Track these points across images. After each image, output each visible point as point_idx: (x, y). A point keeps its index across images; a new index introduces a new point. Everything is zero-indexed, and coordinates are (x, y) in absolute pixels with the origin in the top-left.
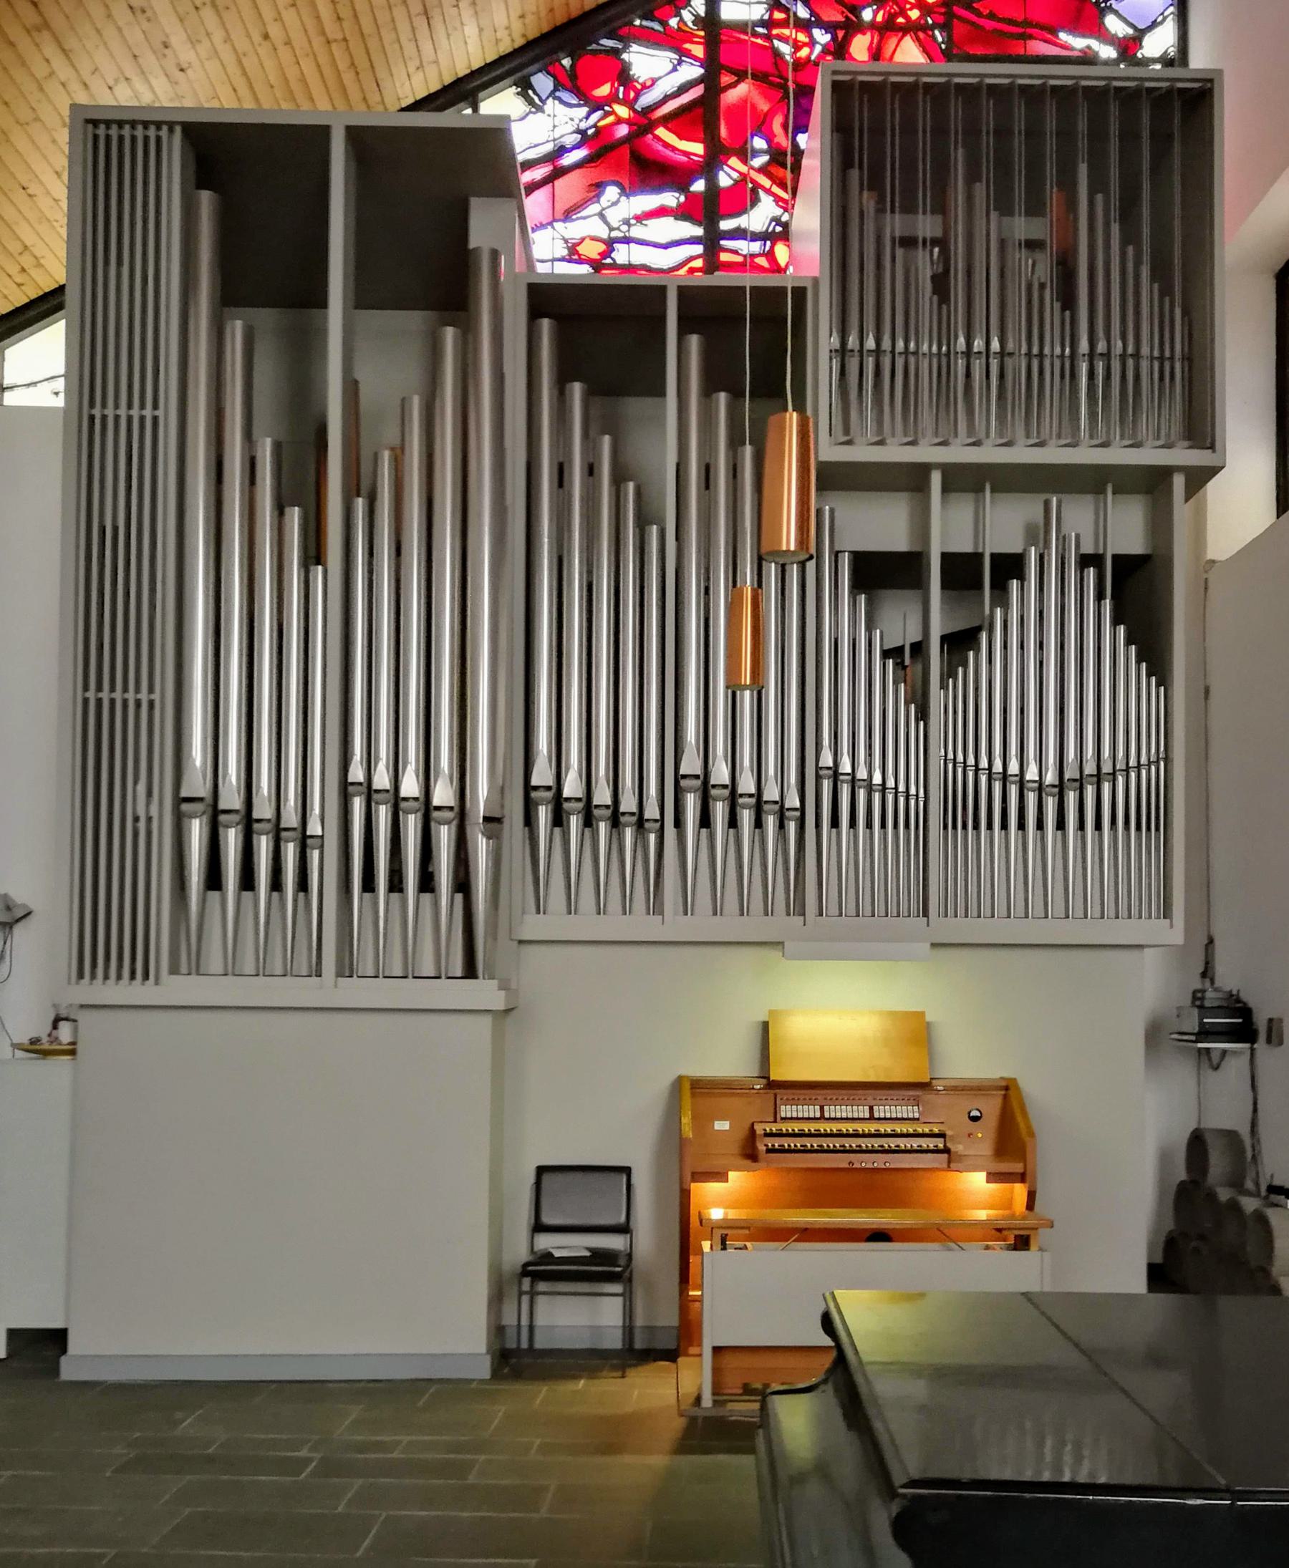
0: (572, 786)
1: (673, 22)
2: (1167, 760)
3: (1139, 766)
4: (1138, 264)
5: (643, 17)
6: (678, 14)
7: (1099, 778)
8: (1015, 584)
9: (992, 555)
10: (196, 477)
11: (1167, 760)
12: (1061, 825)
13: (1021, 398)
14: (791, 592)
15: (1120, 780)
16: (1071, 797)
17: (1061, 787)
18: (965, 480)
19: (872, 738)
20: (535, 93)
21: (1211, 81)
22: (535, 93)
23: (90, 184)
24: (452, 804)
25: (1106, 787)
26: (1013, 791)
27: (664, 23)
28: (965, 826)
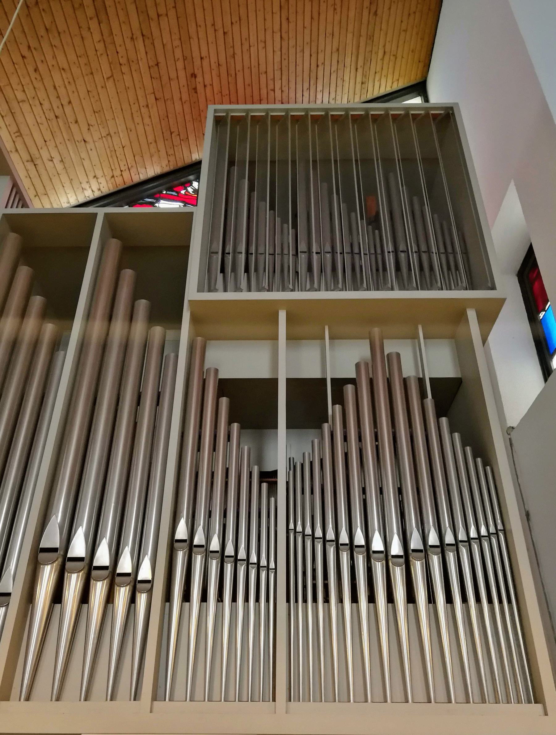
1: (183, 192)
2: (504, 531)
4: (422, 204)
5: (167, 190)
6: (185, 188)
9: (333, 380)
11: (504, 531)
16: (418, 567)
17: (406, 557)
21: (452, 108)
23: (211, 459)
26: (360, 561)
27: (178, 193)
28: (315, 600)
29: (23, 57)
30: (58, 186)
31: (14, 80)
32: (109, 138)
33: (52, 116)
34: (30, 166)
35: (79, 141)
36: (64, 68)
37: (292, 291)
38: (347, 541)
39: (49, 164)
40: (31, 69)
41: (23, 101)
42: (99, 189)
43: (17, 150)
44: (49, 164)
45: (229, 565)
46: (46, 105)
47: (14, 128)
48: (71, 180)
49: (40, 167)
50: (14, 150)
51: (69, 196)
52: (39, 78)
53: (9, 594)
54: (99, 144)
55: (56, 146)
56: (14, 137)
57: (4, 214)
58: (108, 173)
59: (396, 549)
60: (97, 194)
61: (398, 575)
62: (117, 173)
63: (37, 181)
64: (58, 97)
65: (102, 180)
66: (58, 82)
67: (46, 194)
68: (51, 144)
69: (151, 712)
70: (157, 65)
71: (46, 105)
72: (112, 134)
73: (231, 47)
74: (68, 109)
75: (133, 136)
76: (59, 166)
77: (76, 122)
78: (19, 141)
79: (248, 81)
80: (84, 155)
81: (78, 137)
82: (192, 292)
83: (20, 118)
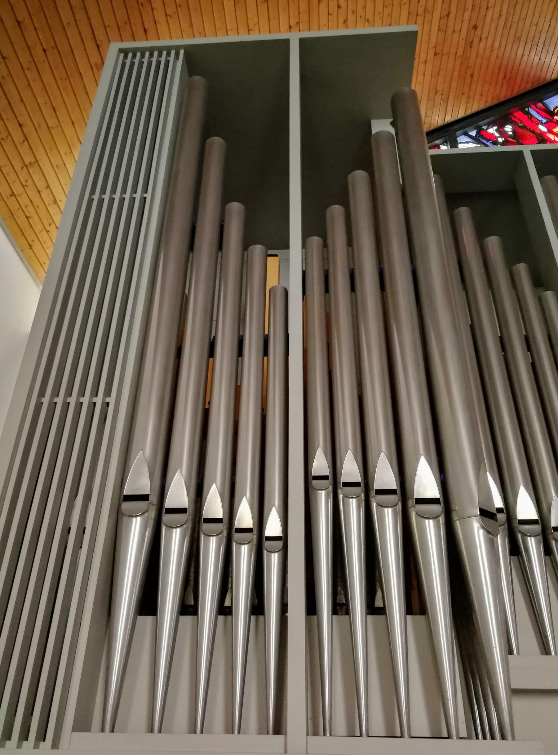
35: (5, 137)
36: (369, 19)
38: (357, 477)
45: (213, 541)
69: (546, 651)
70: (448, 15)
73: (386, 7)
79: (519, 34)
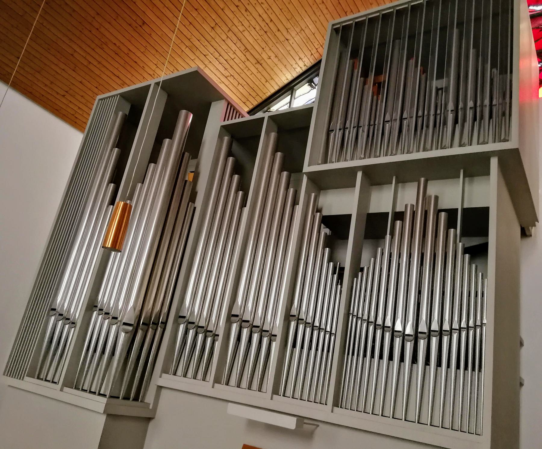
0: (328, 329)
3: (468, 328)
7: (441, 333)
8: (167, 141)
10: (92, 196)
12: (414, 360)
13: (429, 124)
14: (448, 266)
15: (455, 336)
16: (422, 344)
18: (402, 173)
19: (322, 301)
20: (314, 83)
22: (314, 83)
24: (133, 323)
25: (445, 339)
26: (388, 336)
29: (237, 6)
30: (278, 71)
31: (236, 21)
32: (302, 31)
33: (263, 32)
34: (258, 66)
37: (364, 158)
39: (269, 61)
40: (243, 11)
41: (244, 31)
42: (305, 65)
43: (248, 60)
44: (269, 61)
46: (258, 28)
47: (243, 48)
48: (285, 66)
49: (264, 64)
50: (246, 60)
51: (286, 75)
52: (249, 14)
53: (276, 336)
54: (297, 38)
55: (270, 49)
56: (244, 52)
57: (222, 126)
58: (308, 54)
59: (409, 330)
60: (304, 69)
61: (409, 346)
62: (314, 51)
63: (264, 73)
64: (263, 20)
65: (305, 59)
66: (261, 11)
67: (272, 79)
68: (267, 49)
69: (332, 412)
71: (258, 28)
72: (303, 28)
74: (271, 25)
75: (318, 24)
76: (276, 60)
77: (279, 30)
78: (248, 54)
80: (289, 48)
81: (282, 39)
82: (306, 169)
83: (245, 41)
